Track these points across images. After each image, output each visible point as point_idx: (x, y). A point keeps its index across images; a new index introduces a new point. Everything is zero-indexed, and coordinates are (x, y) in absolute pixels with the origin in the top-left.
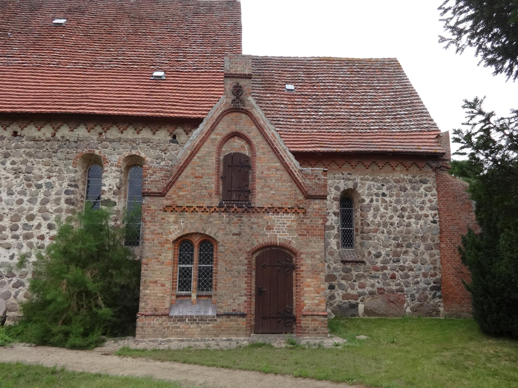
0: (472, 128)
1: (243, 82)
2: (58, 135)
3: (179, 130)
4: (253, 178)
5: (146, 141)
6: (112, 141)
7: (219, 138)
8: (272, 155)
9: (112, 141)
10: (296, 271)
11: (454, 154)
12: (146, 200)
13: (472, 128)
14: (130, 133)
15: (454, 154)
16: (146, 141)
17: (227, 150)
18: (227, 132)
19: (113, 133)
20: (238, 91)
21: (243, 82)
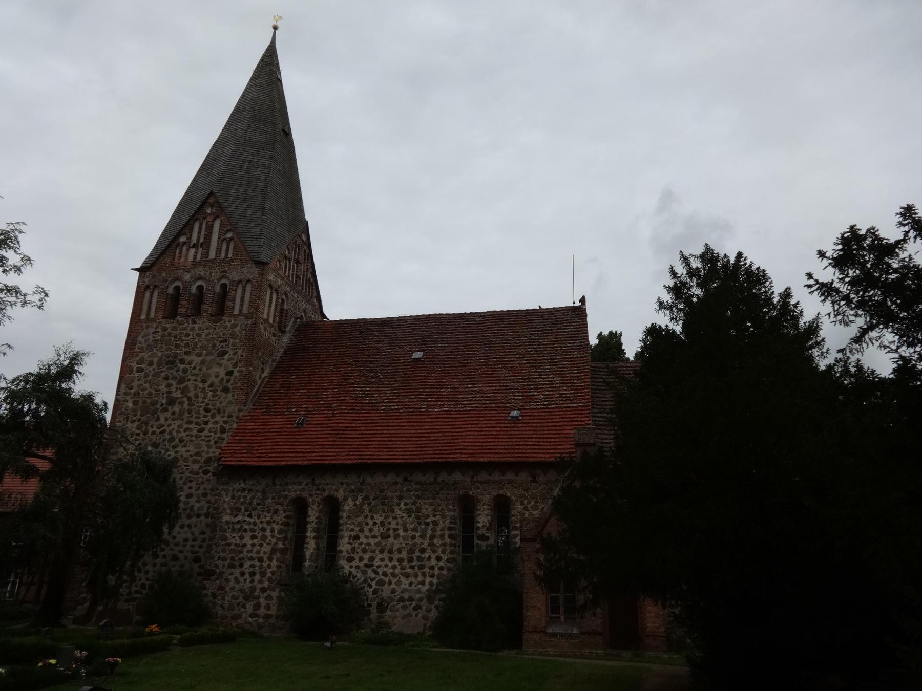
2: (439, 479)
5: (510, 482)
6: (482, 483)
9: (482, 483)
16: (510, 482)
19: (483, 476)
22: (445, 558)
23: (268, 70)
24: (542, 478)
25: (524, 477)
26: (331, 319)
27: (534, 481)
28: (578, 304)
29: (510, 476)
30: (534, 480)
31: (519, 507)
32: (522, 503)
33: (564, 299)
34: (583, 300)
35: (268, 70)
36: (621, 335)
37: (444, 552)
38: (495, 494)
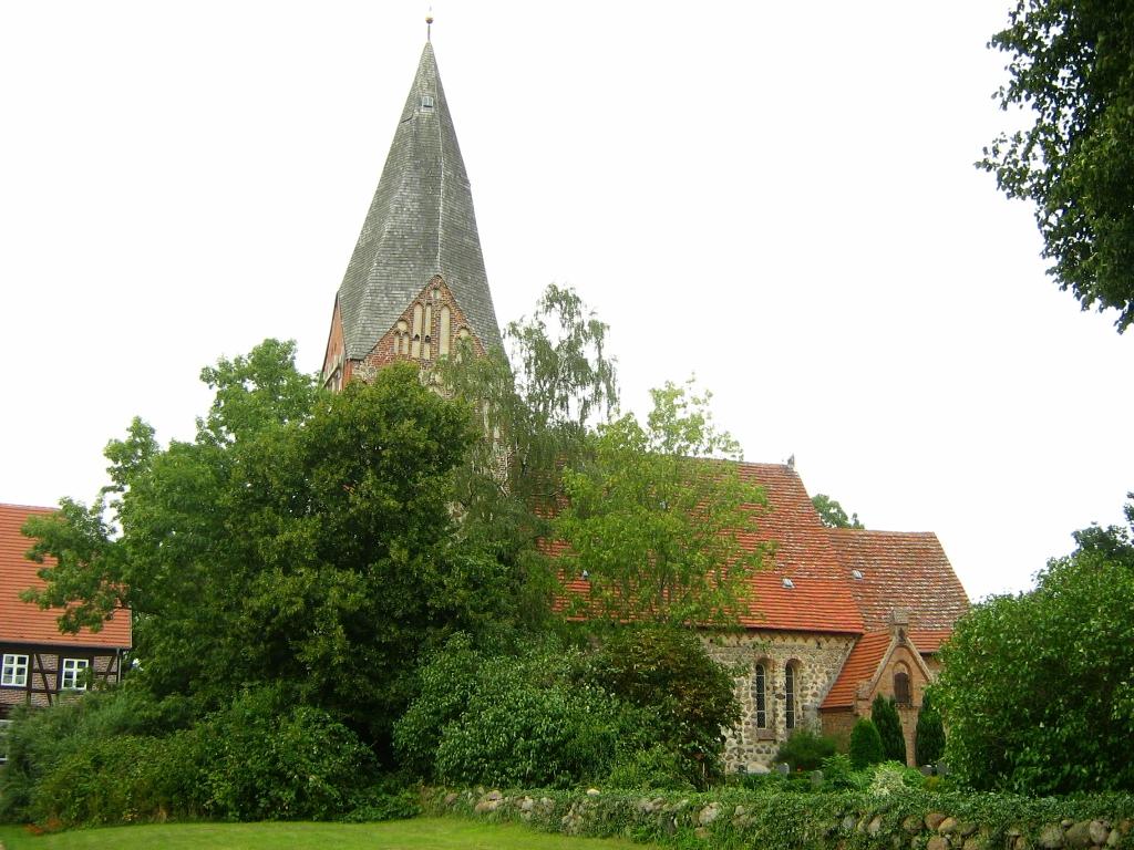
0: (600, 347)
1: (904, 628)
2: (741, 642)
3: (822, 639)
4: (912, 689)
5: (801, 647)
6: (778, 647)
7: (893, 664)
8: (921, 674)
9: (778, 647)
10: (148, 684)
11: (583, 417)
12: (859, 703)
13: (600, 347)
14: (789, 641)
15: (583, 417)
16: (801, 647)
17: (897, 672)
18: (896, 660)
19: (778, 641)
20: (902, 634)
21: (904, 628)
22: (750, 714)
23: (429, 65)
24: (825, 645)
25: (811, 642)
26: (868, 527)
27: (819, 647)
28: (786, 463)
29: (800, 641)
30: (819, 647)
31: (809, 670)
32: (810, 667)
33: (281, 287)
34: (791, 461)
35: (429, 65)
36: (289, 347)
37: (749, 709)
38: (788, 657)
